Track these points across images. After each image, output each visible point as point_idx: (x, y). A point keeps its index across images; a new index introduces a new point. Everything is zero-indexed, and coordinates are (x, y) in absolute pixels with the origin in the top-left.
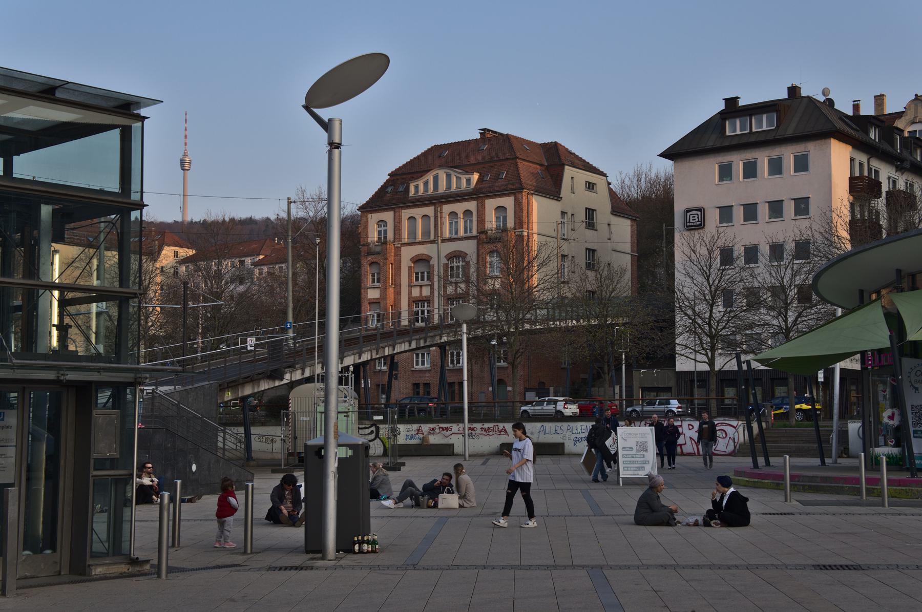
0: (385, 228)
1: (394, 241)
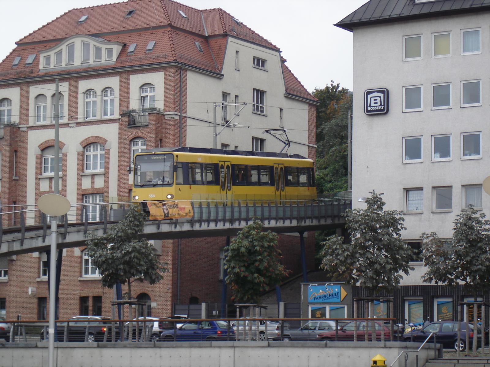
0: (9, 108)
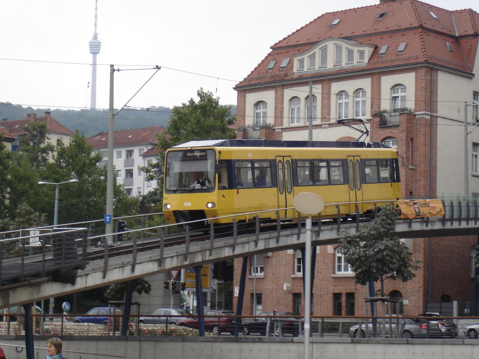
0: (264, 110)
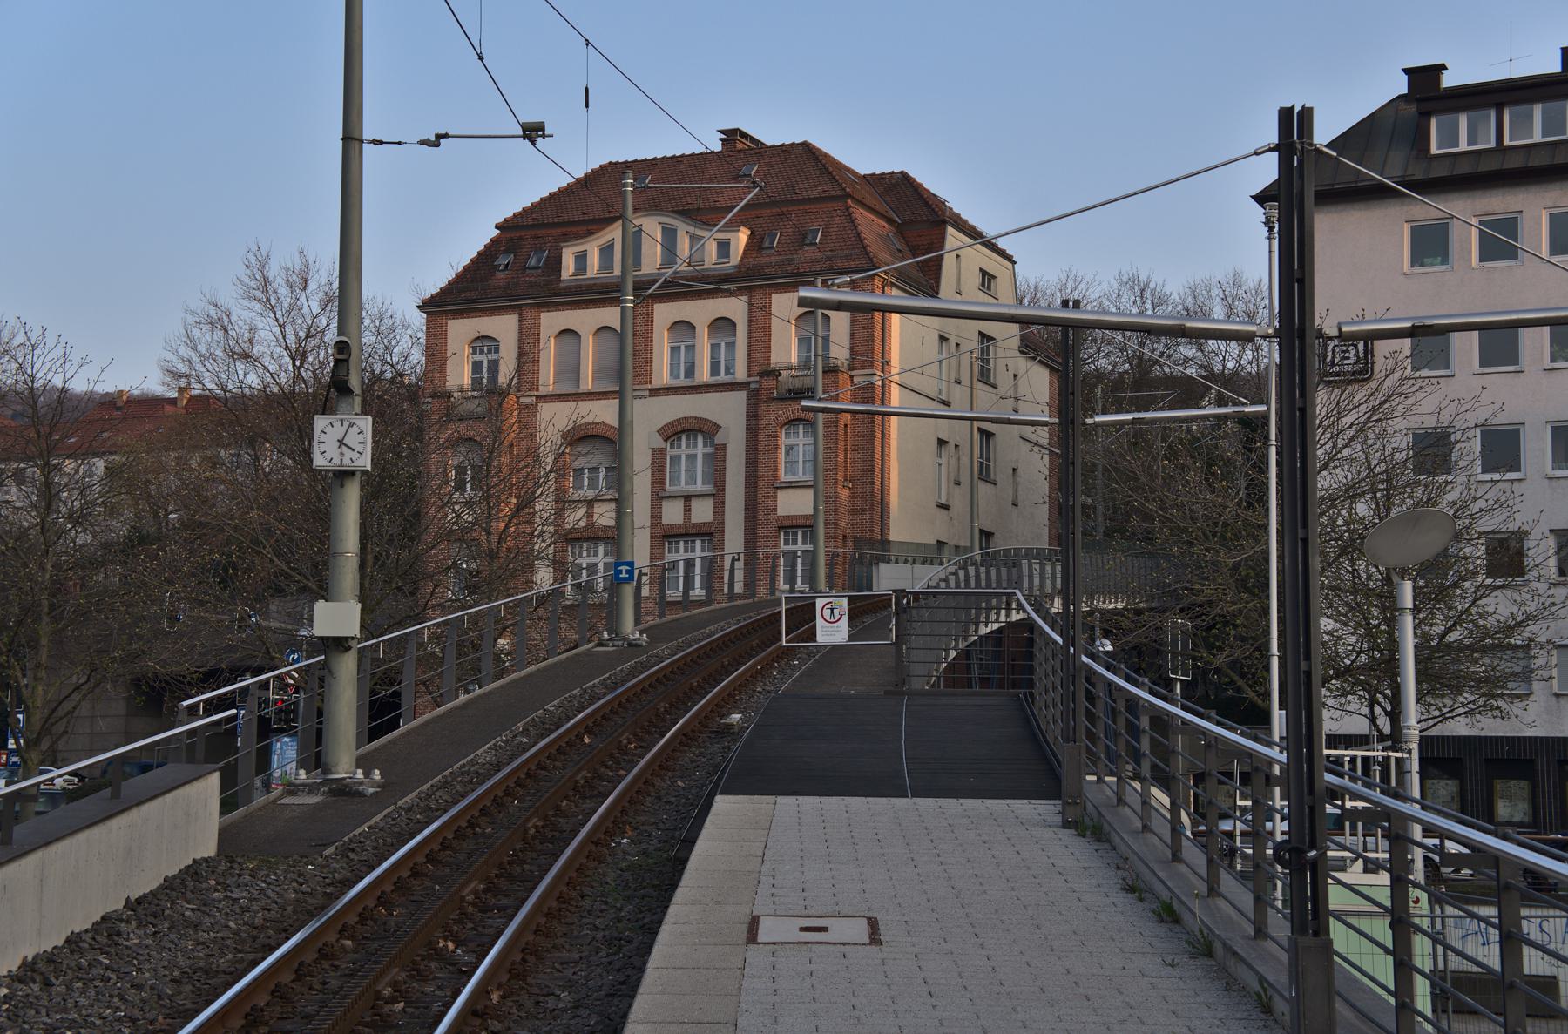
0: (493, 356)
1: (851, 368)
